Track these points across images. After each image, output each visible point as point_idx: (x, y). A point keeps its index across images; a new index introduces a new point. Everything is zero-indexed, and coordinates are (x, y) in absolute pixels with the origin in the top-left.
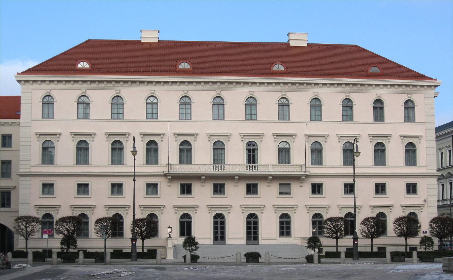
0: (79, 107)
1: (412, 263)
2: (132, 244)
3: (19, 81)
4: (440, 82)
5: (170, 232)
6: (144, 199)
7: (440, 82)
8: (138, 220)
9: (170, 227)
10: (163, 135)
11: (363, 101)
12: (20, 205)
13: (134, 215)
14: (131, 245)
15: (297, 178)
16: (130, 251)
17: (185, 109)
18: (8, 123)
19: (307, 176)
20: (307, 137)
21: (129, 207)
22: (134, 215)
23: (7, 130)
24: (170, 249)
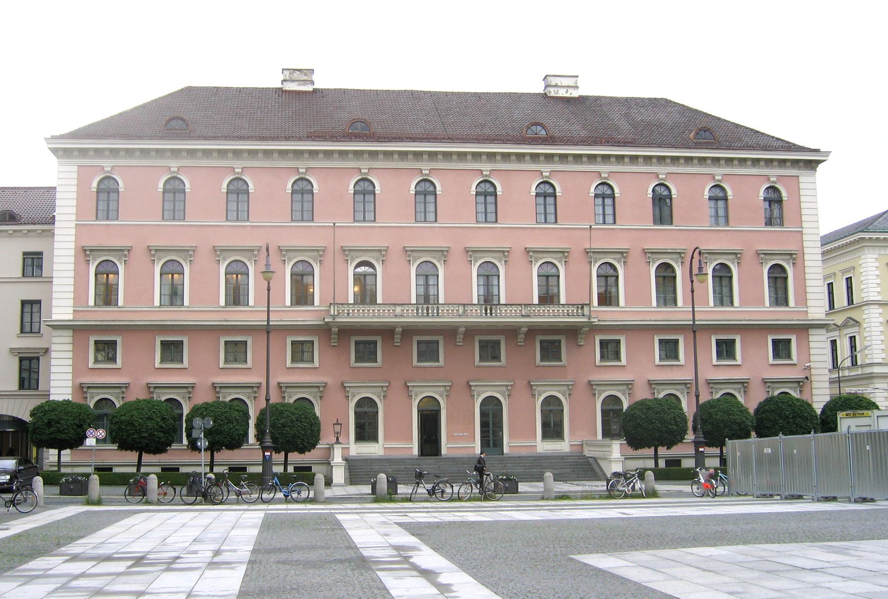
0: (166, 198)
1: (35, 507)
2: (264, 456)
3: (55, 151)
4: (828, 153)
5: (337, 433)
6: (712, 368)
7: (828, 153)
8: (704, 404)
9: (337, 424)
10: (386, 251)
11: (634, 188)
12: (52, 384)
13: (697, 396)
14: (261, 459)
15: (573, 332)
16: (259, 469)
17: (364, 202)
18: (21, 231)
19: (595, 329)
20: (88, 253)
21: (259, 386)
22: (267, 400)
23: (33, 246)
24: (338, 466)
